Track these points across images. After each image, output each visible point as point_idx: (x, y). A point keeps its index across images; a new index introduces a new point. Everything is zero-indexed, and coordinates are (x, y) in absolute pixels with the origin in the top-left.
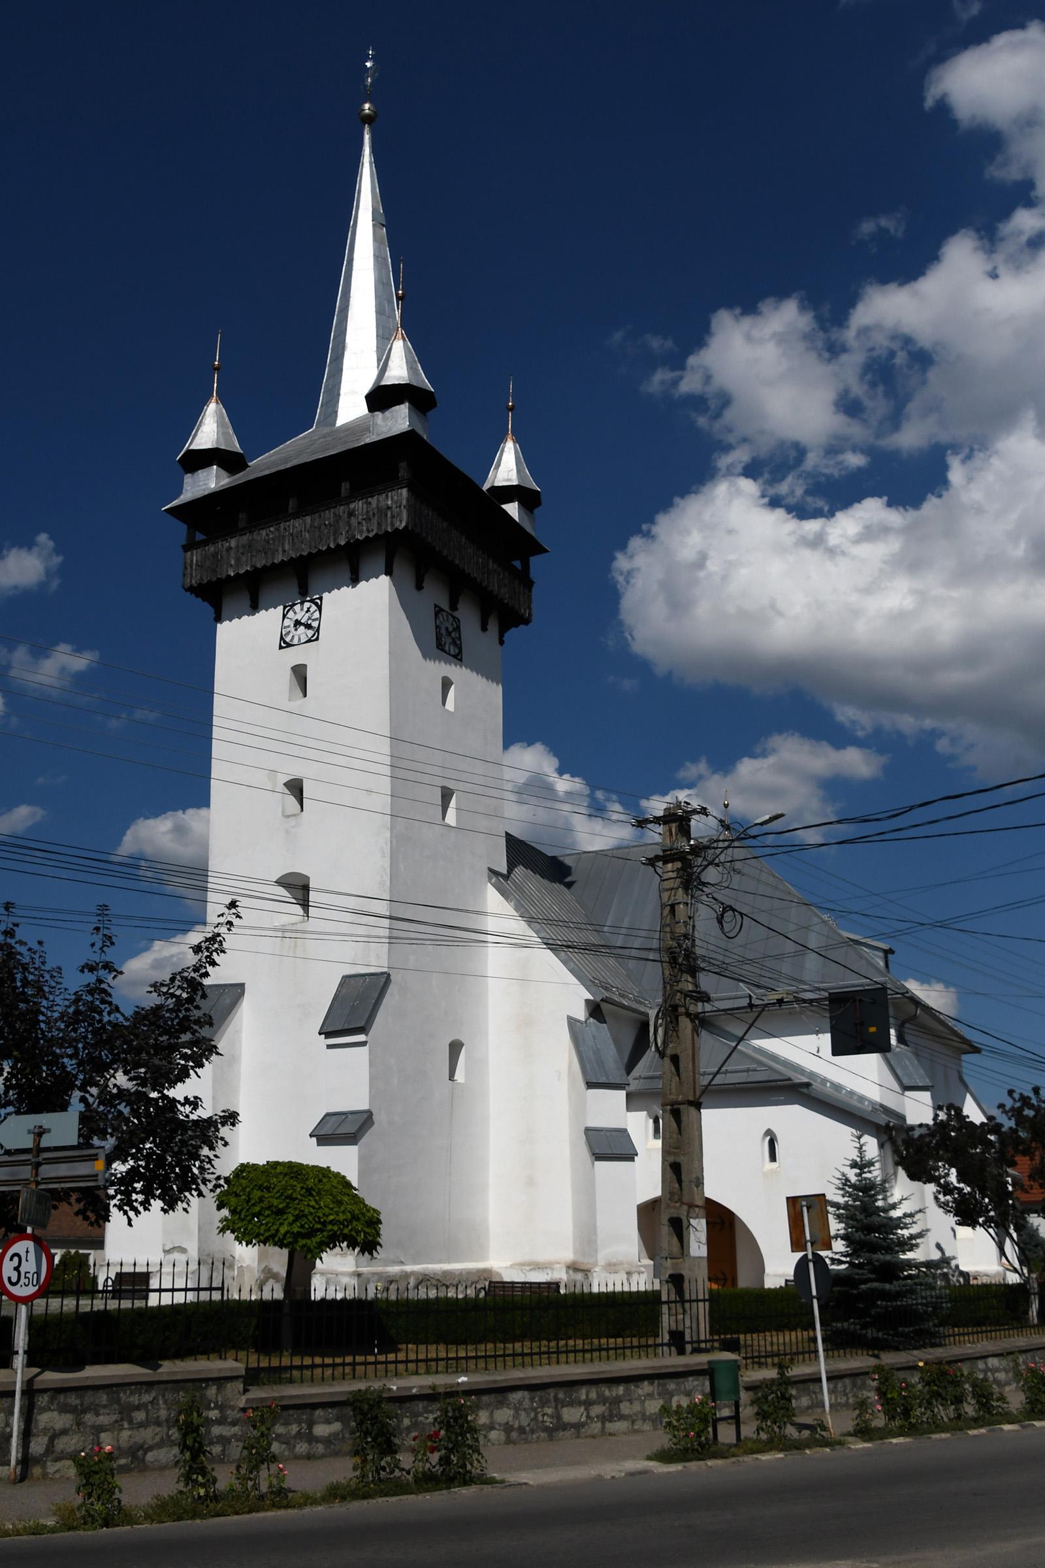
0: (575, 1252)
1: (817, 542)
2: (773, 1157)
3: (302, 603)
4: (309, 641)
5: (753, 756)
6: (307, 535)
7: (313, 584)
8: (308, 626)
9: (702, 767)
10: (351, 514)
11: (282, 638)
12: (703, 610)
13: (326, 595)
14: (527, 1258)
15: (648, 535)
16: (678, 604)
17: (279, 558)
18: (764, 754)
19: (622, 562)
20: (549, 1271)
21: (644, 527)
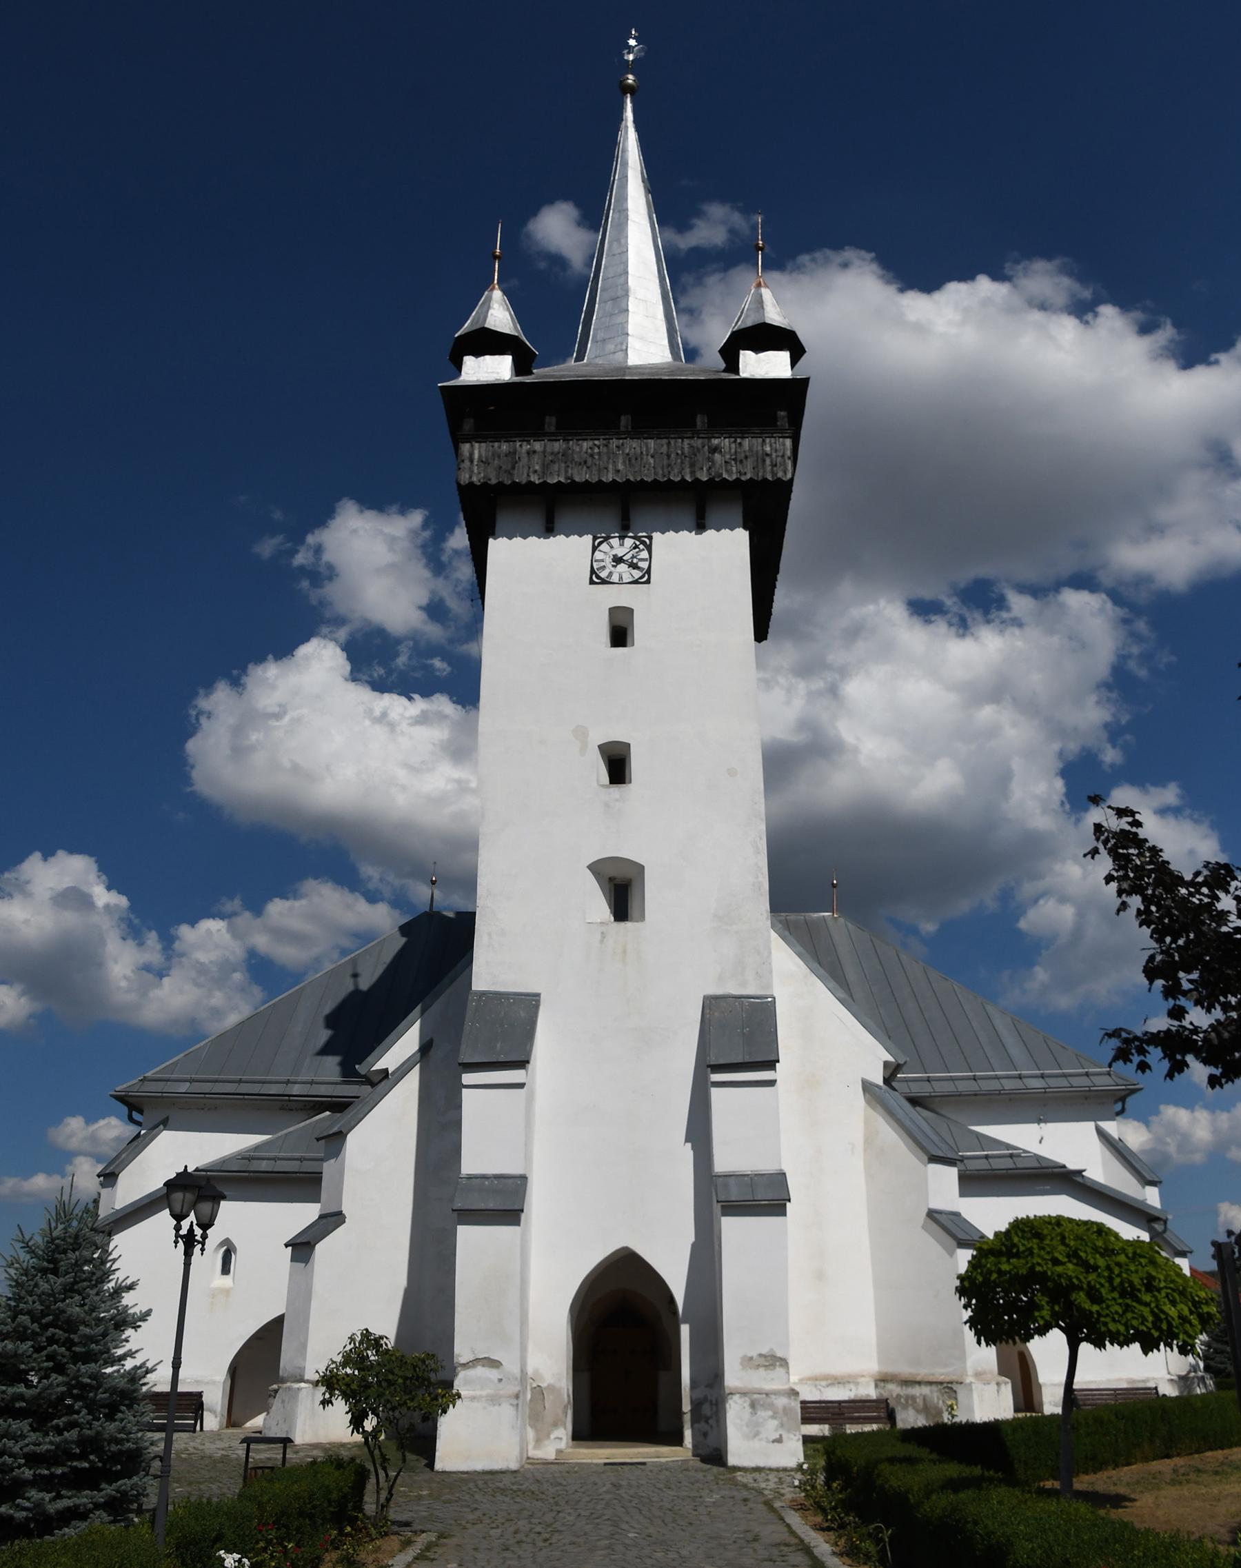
0: (880, 1362)
1: (383, 718)
2: (226, 1270)
3: (622, 538)
4: (636, 582)
5: (284, 896)
6: (652, 461)
7: (637, 518)
8: (634, 566)
9: (236, 903)
10: (715, 450)
11: (593, 571)
12: (259, 759)
13: (657, 536)
14: (818, 1371)
15: (237, 683)
16: (240, 752)
17: (608, 477)
18: (296, 895)
19: (203, 703)
20: (852, 1386)
21: (235, 672)
